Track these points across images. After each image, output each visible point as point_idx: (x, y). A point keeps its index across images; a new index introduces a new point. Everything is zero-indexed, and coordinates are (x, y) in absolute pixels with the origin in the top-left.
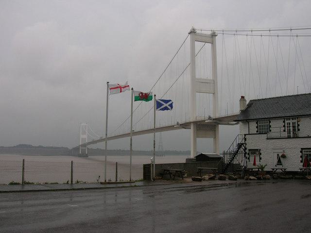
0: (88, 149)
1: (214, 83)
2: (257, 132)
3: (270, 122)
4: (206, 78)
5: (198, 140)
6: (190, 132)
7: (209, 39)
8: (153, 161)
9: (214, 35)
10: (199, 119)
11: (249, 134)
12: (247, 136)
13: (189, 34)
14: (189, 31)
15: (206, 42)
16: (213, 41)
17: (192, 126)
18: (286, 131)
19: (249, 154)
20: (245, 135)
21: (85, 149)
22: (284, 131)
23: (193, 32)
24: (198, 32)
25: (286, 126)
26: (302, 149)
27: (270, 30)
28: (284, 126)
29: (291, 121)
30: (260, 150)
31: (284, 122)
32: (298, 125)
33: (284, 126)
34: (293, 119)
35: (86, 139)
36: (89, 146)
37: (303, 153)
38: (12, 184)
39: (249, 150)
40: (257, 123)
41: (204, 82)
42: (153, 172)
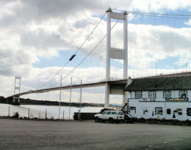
0: (20, 99)
1: (125, 52)
2: (135, 97)
3: (142, 93)
4: (156, 75)
5: (111, 96)
6: (104, 88)
7: (123, 17)
8: (79, 111)
9: (125, 13)
10: (111, 80)
11: (131, 99)
12: (129, 100)
13: (107, 12)
14: (107, 10)
15: (119, 19)
16: (125, 18)
17: (106, 84)
18: (150, 97)
19: (130, 109)
20: (128, 99)
21: (18, 99)
22: (149, 98)
23: (109, 11)
24: (113, 11)
25: (150, 95)
26: (156, 108)
27: (167, 15)
28: (149, 95)
29: (152, 93)
30: (135, 107)
31: (149, 93)
32: (156, 95)
33: (149, 95)
34: (153, 92)
35: (126, 111)
36: (21, 97)
37: (156, 110)
38: (99, 104)
39: (130, 107)
40: (135, 93)
41: (118, 51)
42: (79, 117)
